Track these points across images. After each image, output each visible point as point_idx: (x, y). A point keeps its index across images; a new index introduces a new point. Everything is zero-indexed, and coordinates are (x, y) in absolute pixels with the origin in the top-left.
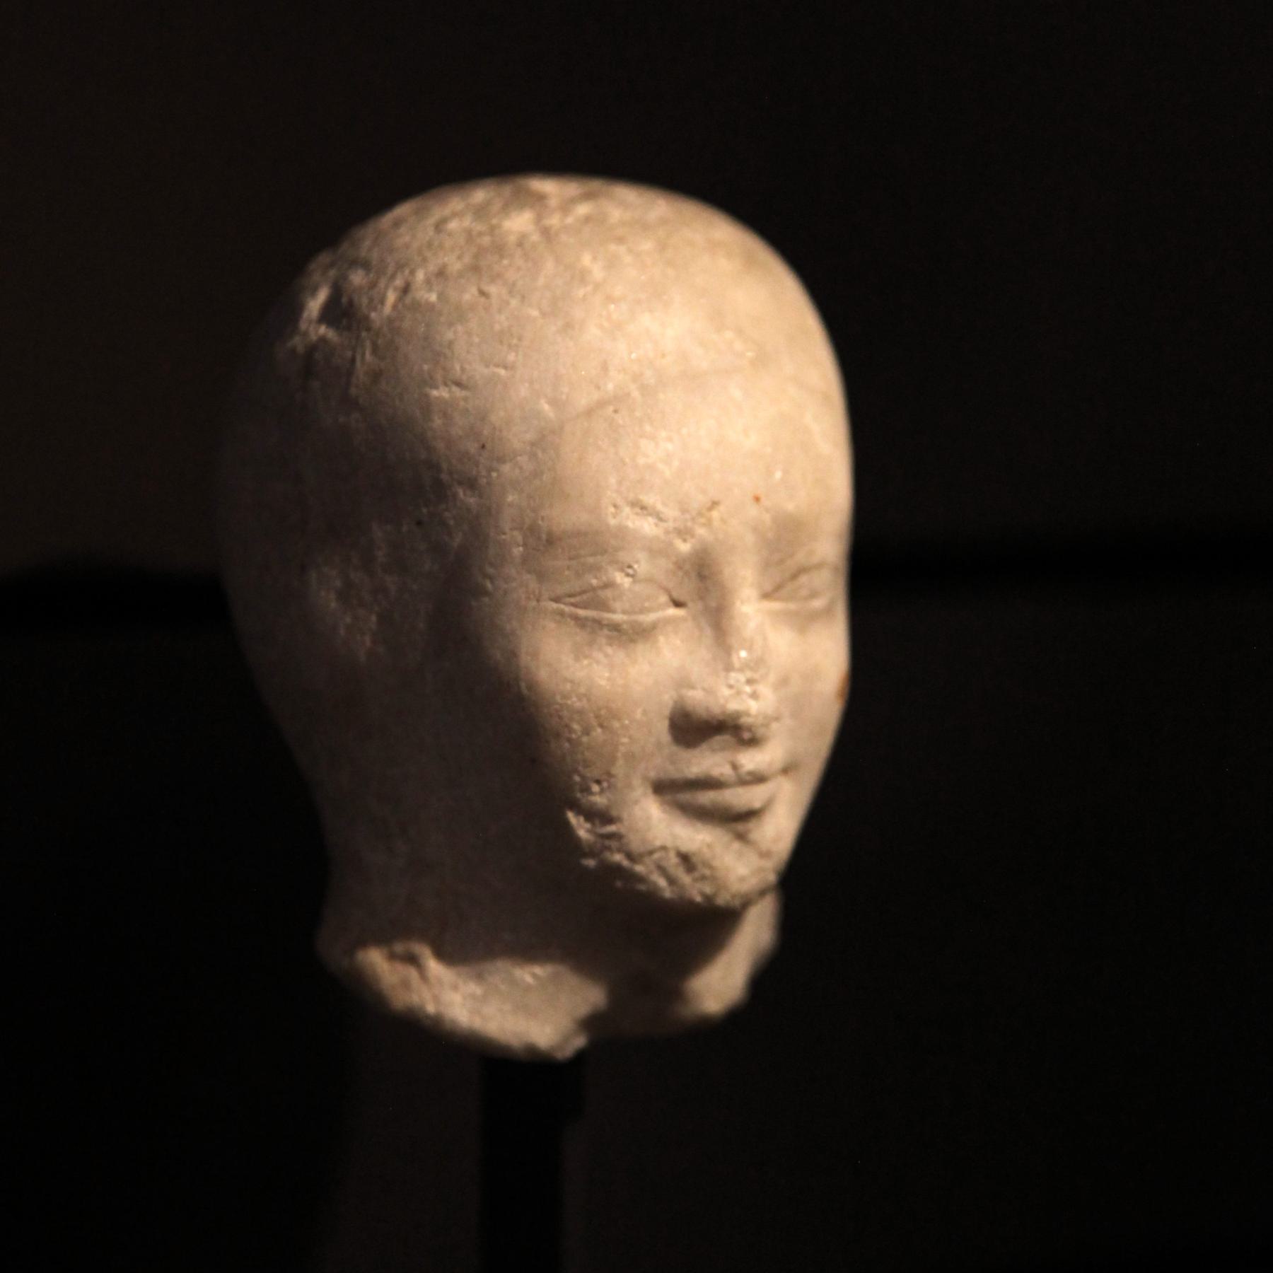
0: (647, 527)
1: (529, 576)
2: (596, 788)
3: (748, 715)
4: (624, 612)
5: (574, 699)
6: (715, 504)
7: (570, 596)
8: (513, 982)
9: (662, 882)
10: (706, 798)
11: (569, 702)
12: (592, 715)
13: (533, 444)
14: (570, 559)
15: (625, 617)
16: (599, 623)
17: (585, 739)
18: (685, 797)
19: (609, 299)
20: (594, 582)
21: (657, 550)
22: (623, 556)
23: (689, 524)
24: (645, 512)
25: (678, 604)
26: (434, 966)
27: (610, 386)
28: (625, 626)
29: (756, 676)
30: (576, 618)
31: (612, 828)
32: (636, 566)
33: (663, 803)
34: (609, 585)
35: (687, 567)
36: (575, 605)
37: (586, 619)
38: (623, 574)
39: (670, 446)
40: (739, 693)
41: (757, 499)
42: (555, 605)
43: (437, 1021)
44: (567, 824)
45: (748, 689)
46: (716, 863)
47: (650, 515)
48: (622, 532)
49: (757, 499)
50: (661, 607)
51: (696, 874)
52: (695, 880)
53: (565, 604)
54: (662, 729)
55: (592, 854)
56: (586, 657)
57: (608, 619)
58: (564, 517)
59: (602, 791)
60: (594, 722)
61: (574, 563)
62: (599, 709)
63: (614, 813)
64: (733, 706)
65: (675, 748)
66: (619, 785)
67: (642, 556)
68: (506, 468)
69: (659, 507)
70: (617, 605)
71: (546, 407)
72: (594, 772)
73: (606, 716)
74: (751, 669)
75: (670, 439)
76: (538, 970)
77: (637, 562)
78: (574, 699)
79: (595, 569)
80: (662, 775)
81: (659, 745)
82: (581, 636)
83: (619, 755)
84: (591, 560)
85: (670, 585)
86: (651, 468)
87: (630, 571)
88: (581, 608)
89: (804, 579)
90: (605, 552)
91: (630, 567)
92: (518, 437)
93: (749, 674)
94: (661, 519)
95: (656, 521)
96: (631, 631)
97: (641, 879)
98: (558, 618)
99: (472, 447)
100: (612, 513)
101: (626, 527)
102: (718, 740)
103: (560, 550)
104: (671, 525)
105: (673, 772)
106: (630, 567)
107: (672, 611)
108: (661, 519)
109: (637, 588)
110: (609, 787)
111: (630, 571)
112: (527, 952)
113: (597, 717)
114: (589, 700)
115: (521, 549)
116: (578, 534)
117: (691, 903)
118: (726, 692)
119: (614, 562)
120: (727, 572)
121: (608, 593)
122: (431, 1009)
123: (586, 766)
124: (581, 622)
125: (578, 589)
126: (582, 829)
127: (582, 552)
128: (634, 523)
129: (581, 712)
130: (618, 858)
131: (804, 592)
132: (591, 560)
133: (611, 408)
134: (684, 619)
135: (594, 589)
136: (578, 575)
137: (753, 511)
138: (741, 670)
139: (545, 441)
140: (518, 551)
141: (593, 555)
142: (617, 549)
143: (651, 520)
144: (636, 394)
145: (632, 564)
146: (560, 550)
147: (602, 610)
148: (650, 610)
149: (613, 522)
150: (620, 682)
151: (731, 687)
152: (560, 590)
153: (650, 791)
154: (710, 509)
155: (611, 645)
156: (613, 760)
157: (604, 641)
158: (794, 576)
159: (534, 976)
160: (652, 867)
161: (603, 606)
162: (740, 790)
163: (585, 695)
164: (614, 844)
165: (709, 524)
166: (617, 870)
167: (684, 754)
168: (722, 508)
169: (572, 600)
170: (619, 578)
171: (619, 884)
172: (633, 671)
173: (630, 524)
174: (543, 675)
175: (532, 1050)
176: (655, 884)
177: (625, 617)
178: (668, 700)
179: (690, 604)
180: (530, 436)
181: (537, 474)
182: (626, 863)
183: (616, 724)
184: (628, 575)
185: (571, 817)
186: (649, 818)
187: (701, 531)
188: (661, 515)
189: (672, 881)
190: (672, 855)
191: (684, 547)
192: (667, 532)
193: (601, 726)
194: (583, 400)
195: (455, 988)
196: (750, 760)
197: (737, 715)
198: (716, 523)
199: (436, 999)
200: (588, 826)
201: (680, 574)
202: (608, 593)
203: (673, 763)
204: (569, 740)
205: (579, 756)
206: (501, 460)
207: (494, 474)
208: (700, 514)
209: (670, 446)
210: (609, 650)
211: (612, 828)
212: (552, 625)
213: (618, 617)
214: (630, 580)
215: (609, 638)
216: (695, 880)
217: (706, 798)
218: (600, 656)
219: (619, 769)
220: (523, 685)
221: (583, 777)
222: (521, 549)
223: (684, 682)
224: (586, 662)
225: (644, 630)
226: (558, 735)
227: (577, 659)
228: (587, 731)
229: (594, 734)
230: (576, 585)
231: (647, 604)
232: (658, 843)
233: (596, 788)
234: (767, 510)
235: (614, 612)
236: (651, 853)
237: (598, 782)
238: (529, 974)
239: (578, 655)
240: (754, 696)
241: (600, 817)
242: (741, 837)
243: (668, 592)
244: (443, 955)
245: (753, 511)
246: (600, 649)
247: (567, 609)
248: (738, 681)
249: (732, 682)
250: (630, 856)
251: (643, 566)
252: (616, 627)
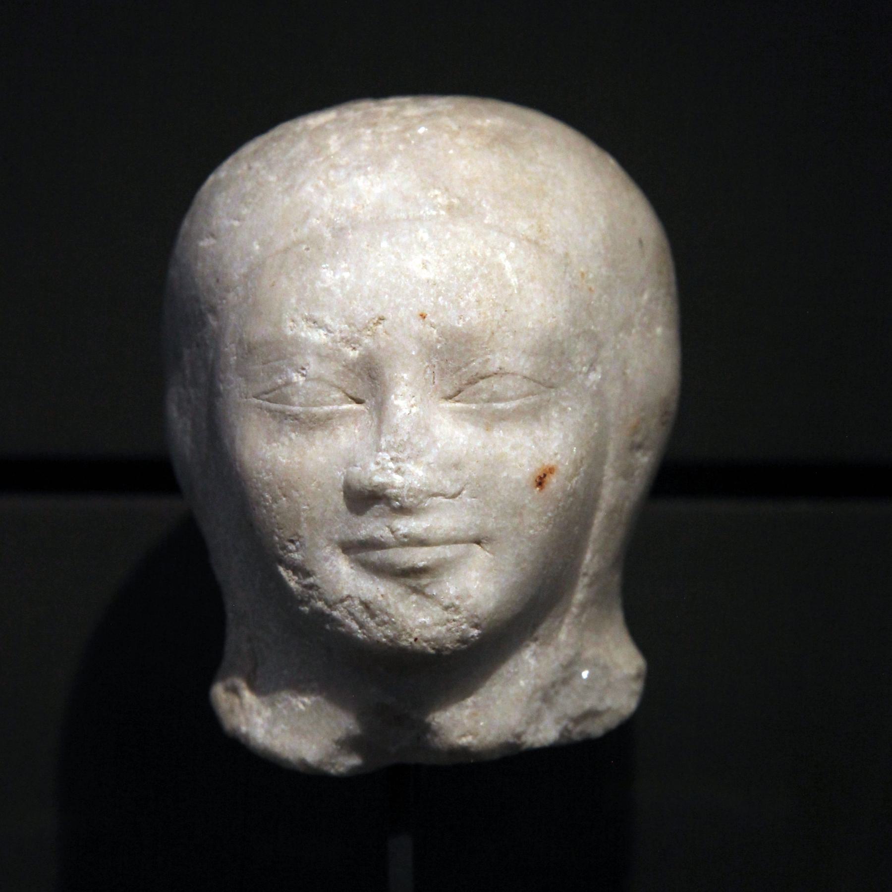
0: (318, 337)
2: (292, 547)
3: (393, 487)
4: (301, 405)
5: (264, 474)
7: (266, 393)
9: (355, 626)
10: (376, 556)
11: (261, 476)
12: (277, 486)
14: (264, 364)
17: (275, 506)
18: (362, 555)
19: (335, 167)
21: (322, 356)
23: (356, 335)
25: (359, 402)
26: (248, 696)
27: (306, 230)
28: (302, 416)
30: (270, 410)
31: (311, 580)
33: (352, 561)
34: (288, 383)
35: (357, 369)
36: (269, 400)
38: (299, 375)
39: (346, 275)
41: (423, 316)
42: (256, 401)
44: (280, 577)
45: (391, 465)
46: (392, 611)
47: (320, 327)
48: (295, 341)
49: (423, 316)
52: (378, 625)
56: (275, 441)
57: (289, 411)
58: (259, 331)
59: (297, 550)
60: (279, 492)
64: (378, 479)
65: (349, 515)
67: (311, 359)
70: (295, 399)
72: (287, 534)
73: (287, 488)
74: (397, 450)
76: (313, 698)
77: (308, 364)
78: (264, 474)
79: (279, 371)
80: (343, 537)
81: (337, 512)
82: (273, 425)
83: (302, 519)
84: (277, 364)
85: (344, 385)
86: (328, 290)
87: (304, 372)
89: (482, 384)
91: (303, 369)
92: (237, 271)
93: (394, 454)
94: (329, 331)
95: (326, 332)
96: (307, 421)
100: (355, 333)
102: (377, 508)
103: (256, 357)
104: (338, 335)
106: (303, 369)
107: (355, 406)
108: (329, 331)
109: (309, 385)
110: (301, 546)
111: (304, 372)
112: (299, 686)
114: (273, 474)
115: (235, 358)
116: (267, 343)
118: (373, 467)
119: (291, 365)
120: (387, 373)
121: (289, 390)
122: (244, 729)
125: (269, 388)
126: (293, 582)
128: (306, 334)
130: (320, 604)
131: (485, 396)
133: (304, 247)
134: (363, 412)
135: (279, 387)
137: (417, 326)
138: (386, 451)
139: (255, 271)
140: (233, 359)
141: (277, 360)
142: (293, 355)
143: (322, 332)
144: (328, 235)
145: (304, 367)
146: (256, 357)
147: (286, 404)
148: (322, 404)
149: (290, 333)
150: (297, 459)
151: (378, 463)
153: (339, 551)
154: (378, 323)
155: (294, 432)
156: (298, 523)
158: (472, 382)
159: (304, 704)
160: (345, 613)
161: (286, 400)
163: (270, 470)
165: (374, 335)
167: (355, 520)
168: (386, 323)
169: (267, 396)
170: (297, 378)
171: (328, 627)
173: (303, 334)
175: (303, 762)
176: (349, 627)
178: (340, 475)
179: (367, 401)
180: (244, 270)
181: (246, 299)
182: (325, 608)
183: (295, 494)
184: (303, 375)
185: (281, 569)
187: (366, 341)
189: (362, 626)
190: (357, 602)
191: (353, 354)
192: (334, 341)
193: (285, 496)
196: (406, 525)
197: (384, 487)
198: (383, 335)
199: (248, 721)
200: (296, 578)
202: (289, 390)
203: (350, 527)
204: (265, 507)
205: (273, 520)
206: (227, 290)
209: (346, 275)
210: (293, 435)
211: (311, 580)
213: (296, 409)
214: (304, 378)
215: (292, 425)
216: (378, 625)
217: (376, 556)
218: (286, 441)
220: (237, 464)
221: (280, 537)
224: (275, 445)
226: (258, 503)
227: (269, 443)
228: (275, 500)
230: (268, 385)
231: (319, 399)
232: (345, 593)
233: (292, 547)
235: (291, 404)
237: (292, 542)
238: (302, 703)
240: (398, 471)
241: (299, 570)
244: (254, 688)
245: (417, 326)
246: (286, 435)
248: (384, 459)
249: (379, 459)
250: (331, 605)
251: (313, 366)
252: (295, 417)
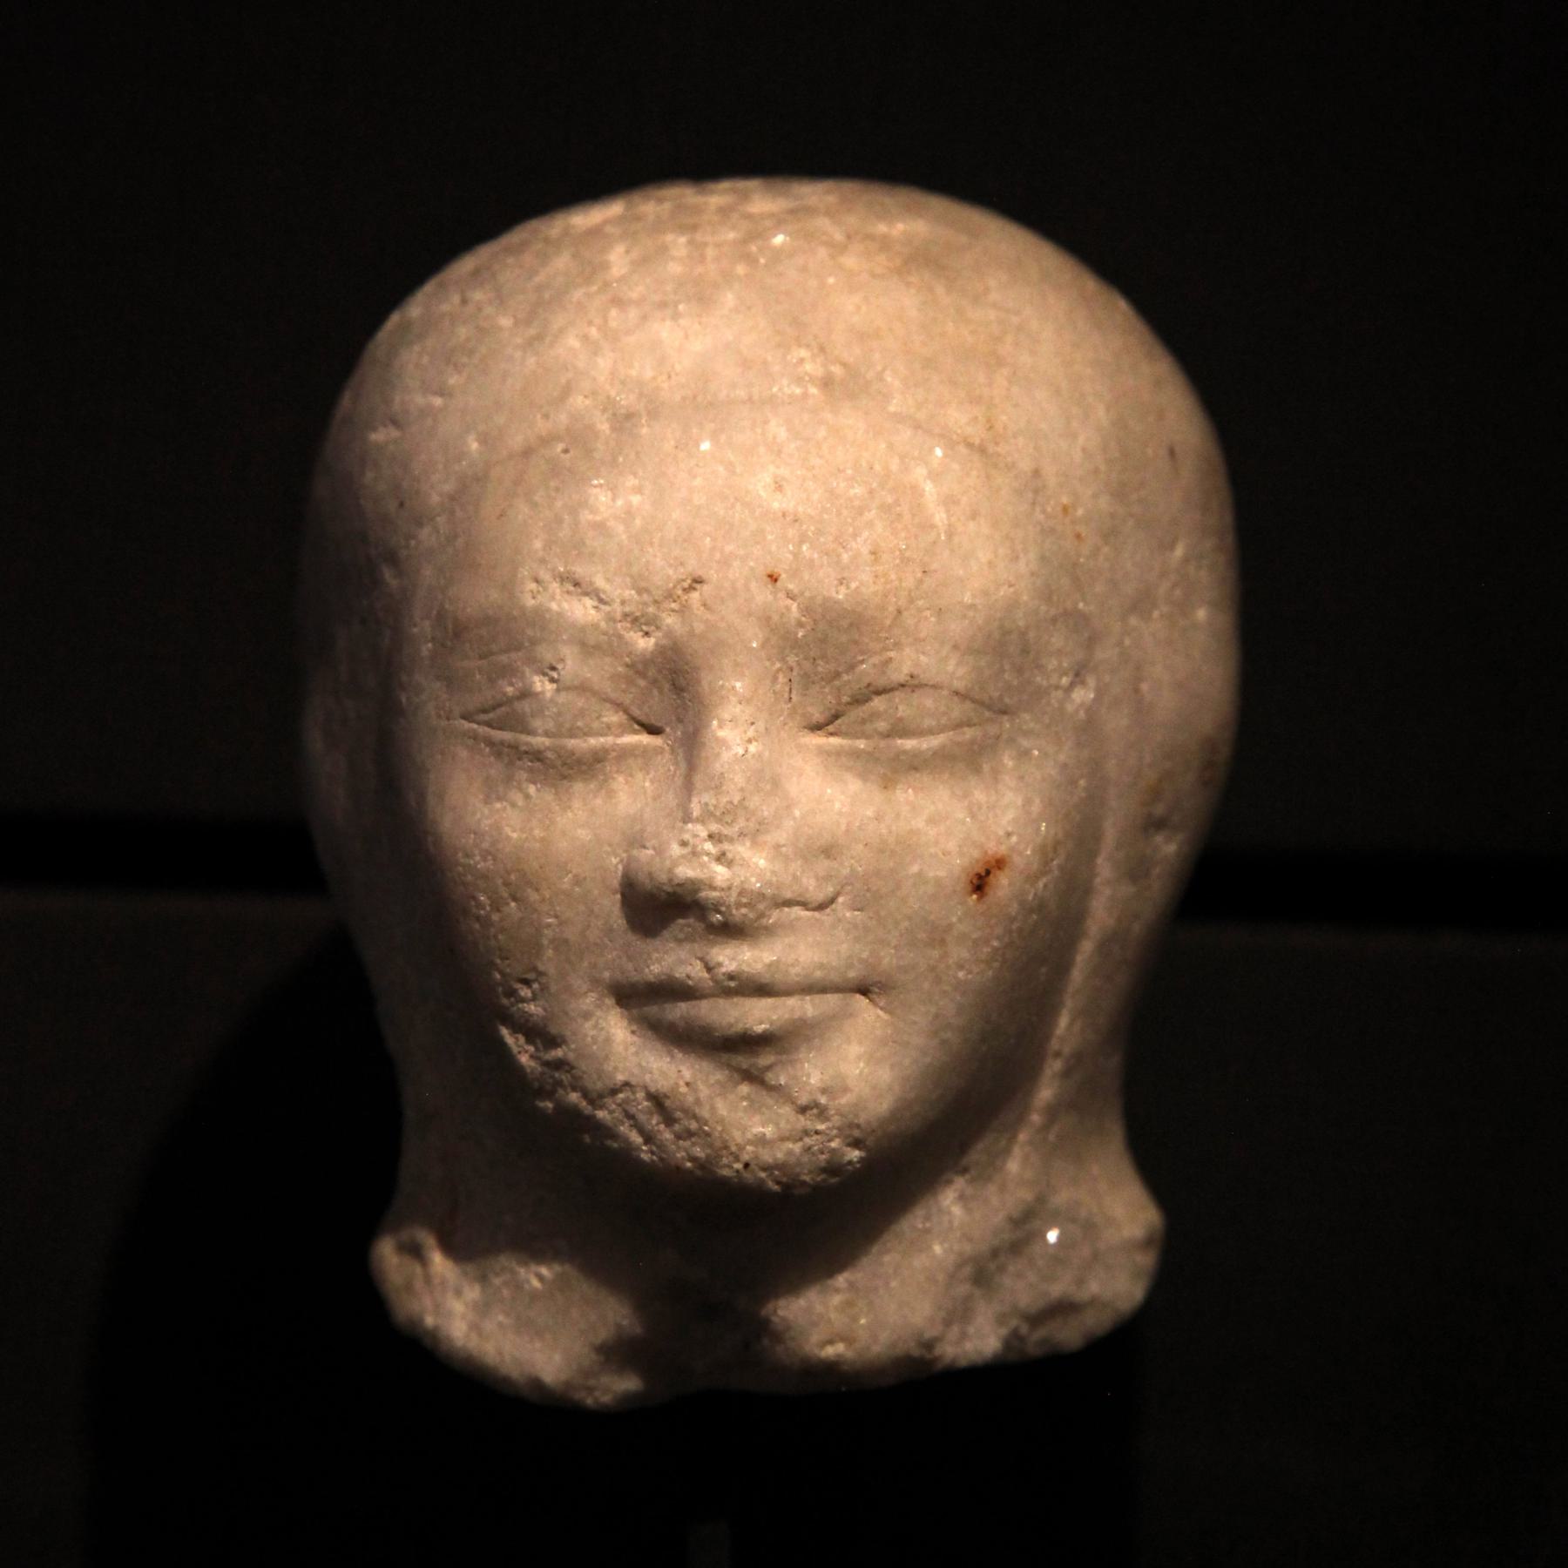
0: (582, 611)
1: (438, 684)
2: (525, 992)
4: (547, 734)
6: (698, 581)
7: (485, 711)
8: (518, 1286)
9: (636, 1138)
10: (678, 1011)
13: (452, 498)
14: (481, 657)
15: (547, 742)
16: (514, 747)
17: (495, 917)
19: (618, 302)
20: (510, 690)
22: (546, 654)
23: (651, 610)
24: (579, 590)
25: (653, 730)
26: (439, 1261)
28: (549, 755)
29: (726, 831)
30: (490, 743)
31: (558, 1053)
32: (560, 666)
33: (631, 1020)
34: (526, 694)
35: (652, 672)
36: (489, 724)
37: (502, 743)
39: (636, 499)
40: (695, 854)
41: (773, 578)
42: (466, 725)
43: (434, 1334)
45: (708, 846)
46: (705, 1113)
47: (586, 594)
48: (540, 620)
49: (773, 578)
50: (607, 730)
51: (677, 1127)
52: (678, 1137)
53: (479, 723)
54: (611, 907)
55: (542, 1093)
56: (499, 799)
57: (527, 744)
59: (534, 999)
61: (484, 663)
62: (508, 873)
63: (553, 1030)
64: (686, 872)
66: (553, 988)
68: (424, 532)
69: (600, 582)
70: (537, 723)
71: (474, 446)
74: (719, 820)
75: (639, 490)
79: (508, 671)
80: (619, 976)
82: (496, 770)
84: (504, 658)
86: (601, 527)
87: (555, 675)
88: (500, 729)
89: (878, 703)
90: (518, 648)
91: (553, 668)
92: (437, 489)
96: (559, 763)
97: (609, 1133)
98: (470, 742)
99: (392, 506)
101: (549, 610)
104: (618, 609)
105: (633, 973)
106: (553, 668)
107: (645, 739)
109: (563, 698)
111: (555, 675)
112: (532, 1248)
113: (507, 884)
115: (430, 645)
116: (488, 620)
117: (679, 1169)
118: (676, 850)
119: (532, 660)
120: (706, 679)
121: (525, 706)
122: (429, 1321)
123: (504, 958)
124: (497, 749)
126: (525, 1056)
127: (494, 647)
128: (559, 606)
129: (485, 876)
130: (574, 1097)
131: (882, 725)
132: (504, 658)
133: (560, 447)
134: (659, 751)
135: (509, 701)
136: (492, 681)
137: (762, 595)
138: (701, 820)
140: (426, 649)
141: (507, 651)
142: (534, 642)
145: (554, 664)
147: (521, 732)
151: (684, 844)
152: (473, 701)
153: (610, 1001)
154: (691, 588)
156: (536, 948)
157: (524, 775)
158: (859, 700)
159: (540, 1278)
161: (519, 724)
162: (722, 1002)
164: (565, 1077)
165: (684, 610)
166: (573, 1113)
170: (541, 685)
172: (564, 820)
173: (554, 606)
174: (446, 823)
175: (537, 1384)
176: (626, 1140)
177: (547, 742)
178: (615, 863)
180: (448, 487)
183: (533, 896)
184: (552, 680)
185: (505, 1032)
186: (608, 1040)
188: (603, 596)
189: (649, 1138)
190: (640, 1095)
191: (644, 644)
192: (610, 619)
193: (515, 899)
194: (517, 440)
195: (458, 1293)
196: (733, 958)
197: (694, 886)
199: (438, 1308)
201: (642, 683)
202: (525, 706)
204: (478, 918)
205: (493, 943)
207: (413, 543)
208: (670, 596)
210: (532, 789)
211: (558, 1053)
212: (463, 754)
213: (539, 741)
214: (555, 686)
215: (531, 770)
216: (678, 1137)
217: (678, 1011)
219: (548, 962)
220: (430, 839)
222: (430, 645)
223: (635, 841)
224: (498, 805)
225: (579, 762)
227: (487, 801)
228: (496, 908)
229: (505, 909)
232: (620, 1077)
233: (525, 992)
234: (791, 596)
236: (614, 1092)
237: (527, 982)
238: (537, 1276)
239: (492, 793)
240: (721, 858)
242: (753, 1077)
243: (619, 706)
244: (451, 1248)
245: (762, 595)
247: (483, 730)
249: (686, 837)
250: (595, 1100)
251: (572, 664)
252: (537, 756)
